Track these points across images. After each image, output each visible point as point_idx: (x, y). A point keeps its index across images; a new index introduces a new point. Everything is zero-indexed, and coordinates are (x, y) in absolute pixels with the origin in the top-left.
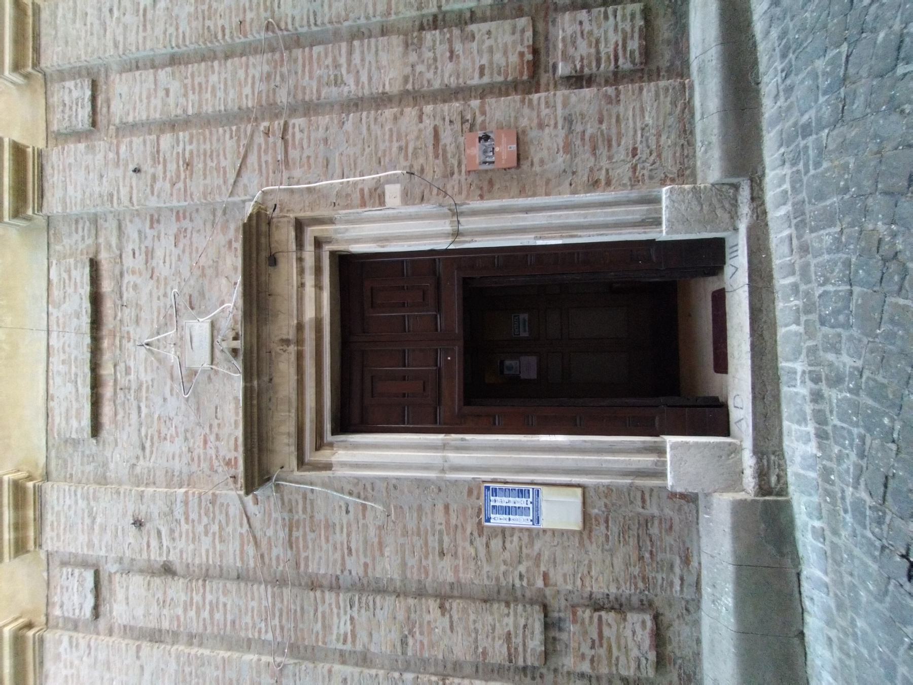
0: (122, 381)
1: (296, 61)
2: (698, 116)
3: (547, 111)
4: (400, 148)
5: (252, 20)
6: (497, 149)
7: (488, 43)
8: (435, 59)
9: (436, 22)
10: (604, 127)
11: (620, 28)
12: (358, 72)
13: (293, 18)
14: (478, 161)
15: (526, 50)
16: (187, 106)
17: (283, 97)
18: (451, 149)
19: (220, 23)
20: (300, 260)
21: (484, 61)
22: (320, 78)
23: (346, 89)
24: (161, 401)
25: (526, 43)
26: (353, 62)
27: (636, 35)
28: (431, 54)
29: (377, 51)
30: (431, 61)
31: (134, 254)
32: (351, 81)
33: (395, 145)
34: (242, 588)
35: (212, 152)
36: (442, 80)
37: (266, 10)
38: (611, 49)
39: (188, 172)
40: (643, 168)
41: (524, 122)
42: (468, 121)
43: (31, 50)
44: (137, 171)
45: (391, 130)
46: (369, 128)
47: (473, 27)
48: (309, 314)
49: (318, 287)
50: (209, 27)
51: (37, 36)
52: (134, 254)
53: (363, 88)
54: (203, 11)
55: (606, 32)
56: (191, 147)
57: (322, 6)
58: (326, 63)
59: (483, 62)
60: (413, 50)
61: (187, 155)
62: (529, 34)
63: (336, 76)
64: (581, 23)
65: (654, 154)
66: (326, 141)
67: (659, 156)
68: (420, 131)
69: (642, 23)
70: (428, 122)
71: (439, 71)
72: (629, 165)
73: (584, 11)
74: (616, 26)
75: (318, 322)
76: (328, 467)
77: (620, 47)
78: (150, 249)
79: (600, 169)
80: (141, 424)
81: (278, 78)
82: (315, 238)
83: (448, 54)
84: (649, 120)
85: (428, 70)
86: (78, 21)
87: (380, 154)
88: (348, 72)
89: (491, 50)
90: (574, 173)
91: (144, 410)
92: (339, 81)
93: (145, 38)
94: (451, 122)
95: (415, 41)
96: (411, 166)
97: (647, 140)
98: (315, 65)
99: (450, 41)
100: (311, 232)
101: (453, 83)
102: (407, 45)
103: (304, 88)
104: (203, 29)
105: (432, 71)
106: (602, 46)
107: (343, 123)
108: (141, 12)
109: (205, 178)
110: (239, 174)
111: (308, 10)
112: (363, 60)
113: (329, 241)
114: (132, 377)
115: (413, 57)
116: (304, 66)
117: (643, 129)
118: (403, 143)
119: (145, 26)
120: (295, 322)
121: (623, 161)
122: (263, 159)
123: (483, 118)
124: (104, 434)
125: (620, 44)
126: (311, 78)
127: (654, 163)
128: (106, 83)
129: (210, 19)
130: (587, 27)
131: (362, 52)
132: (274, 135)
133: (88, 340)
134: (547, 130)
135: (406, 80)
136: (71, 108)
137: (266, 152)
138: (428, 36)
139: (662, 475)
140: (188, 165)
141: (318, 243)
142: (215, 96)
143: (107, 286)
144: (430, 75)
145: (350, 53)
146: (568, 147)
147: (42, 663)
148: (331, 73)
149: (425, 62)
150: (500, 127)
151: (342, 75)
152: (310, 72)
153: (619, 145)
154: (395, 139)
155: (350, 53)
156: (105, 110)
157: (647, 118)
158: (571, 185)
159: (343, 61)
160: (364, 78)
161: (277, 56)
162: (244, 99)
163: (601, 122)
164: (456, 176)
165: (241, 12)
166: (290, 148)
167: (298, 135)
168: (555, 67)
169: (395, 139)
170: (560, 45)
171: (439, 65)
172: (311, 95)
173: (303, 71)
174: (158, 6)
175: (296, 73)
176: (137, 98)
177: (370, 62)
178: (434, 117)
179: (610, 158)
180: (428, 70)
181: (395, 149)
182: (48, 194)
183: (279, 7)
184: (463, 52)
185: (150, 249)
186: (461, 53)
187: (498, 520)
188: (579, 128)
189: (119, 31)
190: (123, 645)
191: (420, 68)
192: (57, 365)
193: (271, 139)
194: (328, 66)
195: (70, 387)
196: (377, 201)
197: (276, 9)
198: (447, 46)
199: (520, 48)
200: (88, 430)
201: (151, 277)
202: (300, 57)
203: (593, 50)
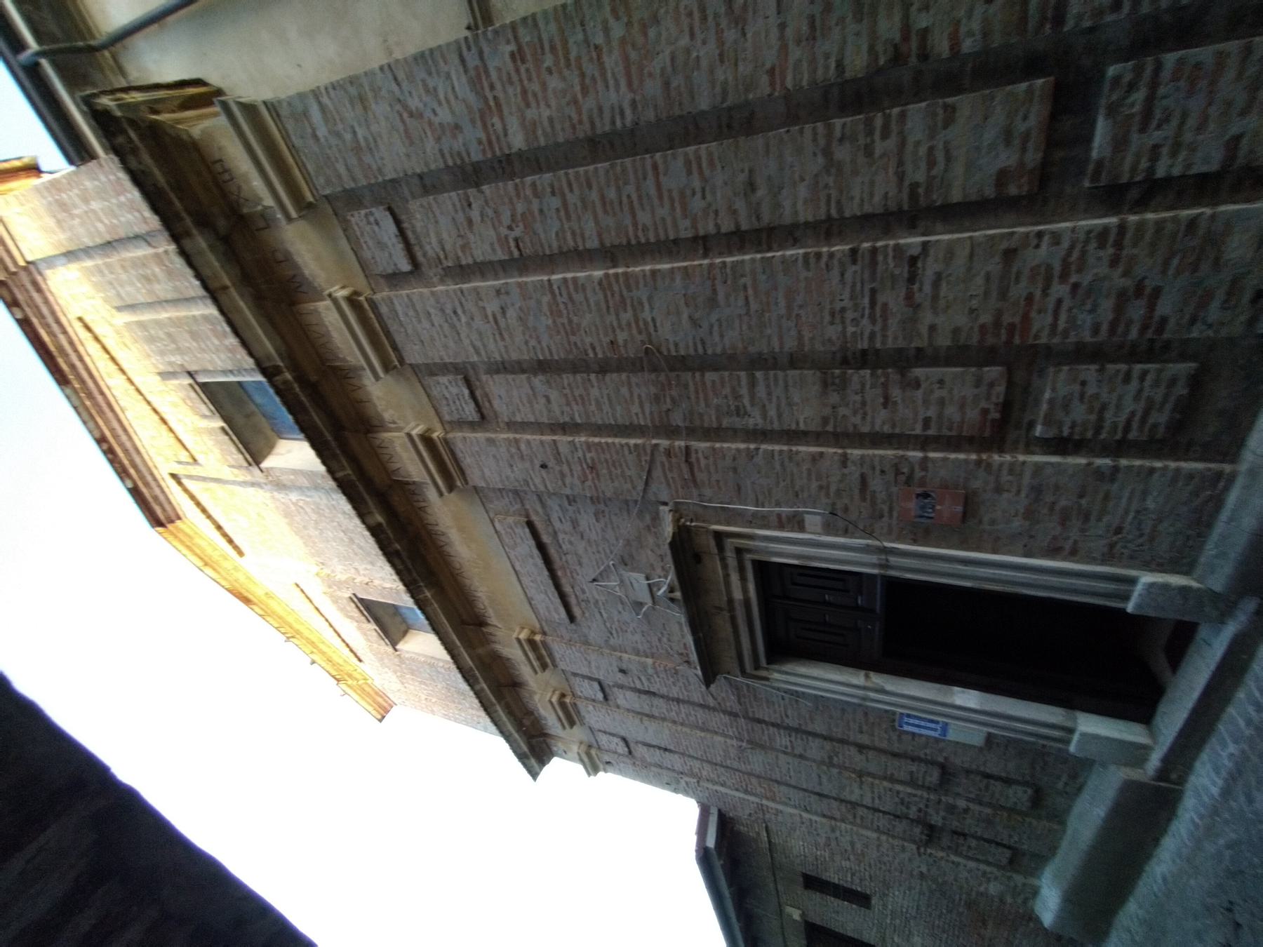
1: (686, 386)
2: (1224, 515)
3: (1010, 478)
4: (821, 487)
7: (938, 393)
8: (864, 404)
10: (1083, 502)
11: (1145, 394)
12: (764, 406)
14: (913, 514)
15: (992, 407)
16: (573, 414)
18: (881, 496)
19: (588, 340)
20: (723, 559)
21: (932, 412)
22: (718, 408)
25: (994, 399)
27: (1168, 407)
29: (786, 386)
30: (858, 405)
32: (756, 413)
35: (614, 462)
37: (640, 333)
38: (1123, 418)
39: (594, 475)
40: (1125, 547)
41: (976, 484)
44: (544, 466)
45: (809, 470)
46: (782, 464)
47: (919, 372)
48: (738, 595)
49: (743, 579)
50: (575, 344)
51: (388, 334)
53: (772, 423)
55: (1120, 398)
57: (711, 333)
58: (724, 393)
59: (929, 413)
60: (834, 391)
62: (1000, 389)
64: (1083, 383)
65: (1145, 538)
66: (735, 470)
67: (1152, 539)
69: (1185, 392)
70: (853, 468)
71: (869, 418)
72: (1104, 542)
73: (1094, 367)
74: (1140, 391)
75: (747, 603)
76: (767, 679)
77: (1137, 418)
79: (1068, 538)
83: (882, 400)
84: (1150, 504)
87: (797, 488)
88: (752, 405)
89: (942, 402)
90: (1031, 537)
91: (605, 615)
92: (742, 412)
93: (506, 347)
94: (883, 472)
95: (837, 381)
96: (834, 504)
98: (711, 394)
102: (825, 384)
103: (701, 415)
105: (859, 417)
106: (1109, 415)
108: (491, 319)
110: (647, 483)
111: (694, 338)
112: (769, 394)
113: (749, 551)
114: (588, 594)
115: (834, 398)
116: (697, 392)
117: (1138, 512)
119: (501, 334)
122: (669, 475)
123: (923, 473)
124: (609, 698)
126: (707, 405)
129: (574, 334)
130: (1091, 390)
131: (768, 386)
132: (676, 457)
133: (546, 573)
134: (1005, 495)
135: (825, 421)
139: (1068, 742)
141: (739, 551)
143: (546, 539)
145: (753, 384)
146: (1029, 514)
147: (579, 712)
149: (851, 406)
150: (945, 486)
151: (744, 407)
152: (706, 399)
156: (487, 404)
159: (744, 391)
160: (772, 413)
161: (662, 378)
163: (1081, 496)
164: (885, 519)
165: (610, 331)
166: (696, 470)
167: (703, 462)
168: (1031, 425)
171: (868, 408)
172: (711, 420)
173: (698, 398)
174: (508, 315)
177: (778, 397)
178: (861, 465)
179: (1083, 530)
180: (855, 413)
181: (814, 485)
182: (468, 472)
183: (656, 331)
186: (899, 400)
187: (906, 728)
188: (1049, 498)
189: (474, 337)
190: (432, 202)
191: (843, 411)
193: (674, 460)
195: (543, 596)
198: (879, 391)
199: (983, 404)
200: (567, 621)
202: (691, 384)
203: (1093, 417)
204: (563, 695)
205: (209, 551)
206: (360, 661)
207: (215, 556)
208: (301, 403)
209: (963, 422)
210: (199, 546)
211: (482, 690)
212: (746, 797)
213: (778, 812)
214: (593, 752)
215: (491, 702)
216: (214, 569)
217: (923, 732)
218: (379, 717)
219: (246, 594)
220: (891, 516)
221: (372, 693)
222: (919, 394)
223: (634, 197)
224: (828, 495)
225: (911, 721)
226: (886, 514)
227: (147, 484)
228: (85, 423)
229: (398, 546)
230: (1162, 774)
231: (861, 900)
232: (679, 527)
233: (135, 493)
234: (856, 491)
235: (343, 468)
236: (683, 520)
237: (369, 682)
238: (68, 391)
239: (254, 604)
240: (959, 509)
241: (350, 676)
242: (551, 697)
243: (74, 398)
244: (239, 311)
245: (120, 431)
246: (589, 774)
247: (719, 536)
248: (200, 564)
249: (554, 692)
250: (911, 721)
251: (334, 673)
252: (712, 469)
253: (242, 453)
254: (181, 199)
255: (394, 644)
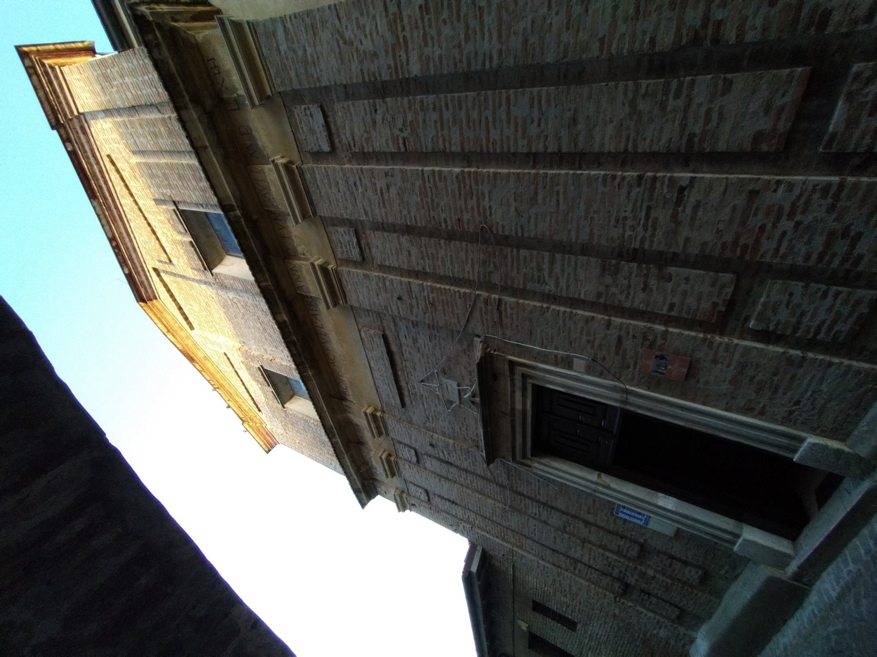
0: (412, 391)
1: (506, 257)
4: (588, 341)
5: (468, 220)
6: (669, 367)
7: (683, 287)
9: (636, 255)
10: (776, 378)
12: (558, 278)
13: (503, 227)
15: (721, 302)
16: (425, 266)
17: (496, 279)
19: (443, 216)
21: (676, 300)
23: (547, 287)
24: (434, 406)
26: (555, 270)
27: (851, 320)
28: (626, 282)
31: (406, 337)
32: (552, 283)
33: (584, 338)
34: (424, 147)
35: (448, 302)
36: (633, 302)
37: (479, 215)
39: (433, 309)
42: (649, 340)
43: (308, 204)
45: (582, 327)
46: (564, 321)
47: (672, 270)
48: (519, 406)
51: (308, 193)
52: (406, 337)
53: (561, 291)
54: (427, 203)
56: (433, 295)
57: (529, 222)
61: (431, 299)
62: (729, 290)
63: (539, 276)
64: (791, 295)
66: (530, 320)
68: (606, 335)
75: (524, 412)
76: (529, 466)
78: (415, 337)
80: (425, 410)
81: (492, 265)
82: (522, 374)
83: (642, 286)
84: (824, 388)
85: (622, 292)
86: (333, 187)
88: (550, 277)
89: (685, 293)
90: (733, 398)
92: (542, 281)
94: (634, 336)
96: (596, 354)
97: (814, 401)
99: (647, 276)
100: (519, 370)
101: (642, 307)
102: (604, 269)
103: (513, 279)
104: (430, 217)
106: (805, 320)
107: (544, 312)
108: (379, 191)
109: (445, 316)
112: (563, 271)
113: (531, 377)
116: (512, 263)
117: (814, 392)
118: (591, 338)
119: (384, 203)
120: (510, 408)
121: (783, 405)
122: (484, 317)
123: (662, 342)
125: (828, 322)
127: (813, 415)
128: (364, 233)
130: (796, 300)
134: (719, 366)
135: (599, 295)
136: (346, 246)
137: (486, 313)
138: (627, 267)
140: (432, 304)
141: (524, 376)
142: (445, 266)
143: (394, 348)
144: (622, 297)
145: (552, 262)
147: (399, 468)
148: (535, 273)
151: (544, 277)
152: (518, 269)
153: (785, 393)
154: (584, 333)
155: (552, 262)
156: (368, 251)
157: (823, 386)
158: (727, 403)
159: (546, 266)
160: (563, 284)
162: (467, 274)
166: (503, 316)
167: (509, 311)
168: (747, 319)
169: (584, 333)
170: (759, 307)
171: (632, 291)
173: (512, 266)
175: (506, 265)
176: (389, 251)
177: (569, 274)
180: (622, 292)
182: (348, 295)
183: (491, 215)
184: (657, 288)
185: (415, 337)
186: (655, 288)
187: (620, 515)
191: (613, 290)
192: (376, 374)
193: (489, 307)
194: (533, 268)
196: (567, 365)
197: (488, 217)
199: (715, 299)
201: (419, 351)
204: (390, 455)
205: (172, 323)
206: (260, 410)
207: (176, 326)
208: (245, 233)
209: (698, 309)
210: (166, 319)
211: (337, 442)
212: (503, 543)
213: (522, 557)
214: (404, 496)
215: (341, 451)
216: (173, 336)
217: (632, 519)
218: (267, 450)
219: (192, 355)
220: (635, 368)
221: (264, 433)
222: (670, 285)
223: (490, 119)
224: (593, 346)
225: (625, 511)
226: (632, 367)
227: (138, 273)
228: (103, 226)
229: (294, 338)
230: (797, 577)
231: (571, 625)
232: (486, 354)
233: (130, 278)
234: (613, 349)
235: (266, 280)
236: (489, 349)
237: (264, 425)
238: (95, 203)
239: (196, 362)
240: (685, 370)
241: (252, 420)
242: (382, 455)
243: (98, 209)
244: (212, 163)
245: (127, 240)
246: (399, 510)
247: (512, 364)
248: (165, 331)
249: (384, 452)
250: (625, 511)
251: (242, 416)
252: (515, 318)
253: (201, 261)
254: (184, 83)
255: (283, 404)
